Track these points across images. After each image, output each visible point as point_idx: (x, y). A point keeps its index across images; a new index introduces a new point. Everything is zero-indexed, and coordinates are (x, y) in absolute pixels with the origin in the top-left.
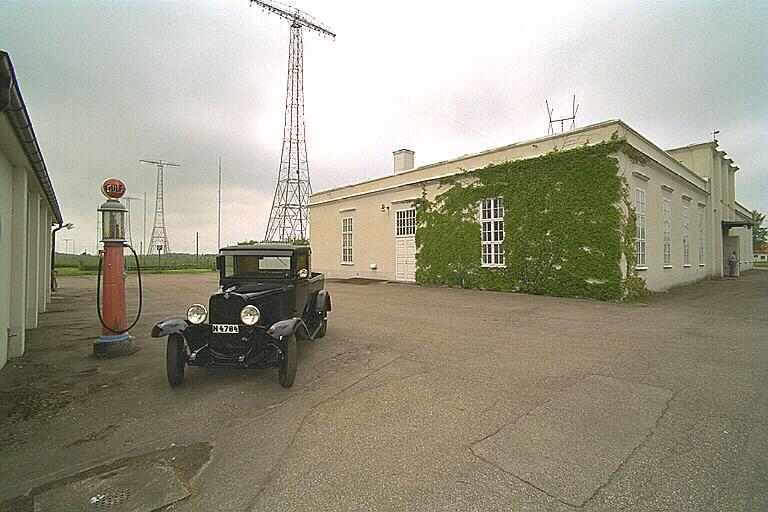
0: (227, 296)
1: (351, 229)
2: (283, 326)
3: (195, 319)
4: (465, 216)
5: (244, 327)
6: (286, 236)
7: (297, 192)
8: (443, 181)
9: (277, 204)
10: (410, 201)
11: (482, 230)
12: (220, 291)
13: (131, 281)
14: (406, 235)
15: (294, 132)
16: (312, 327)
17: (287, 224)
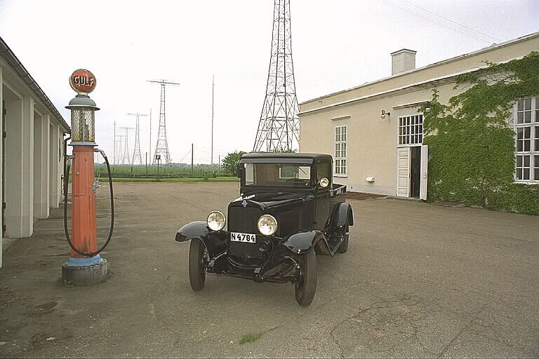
0: (245, 204)
1: (344, 138)
2: (301, 239)
3: (215, 226)
4: (491, 120)
5: (260, 237)
6: (272, 148)
7: (284, 104)
8: (460, 79)
9: (264, 117)
10: (417, 105)
11: (515, 137)
12: (240, 199)
13: (103, 188)
14: (402, 145)
15: (281, 47)
16: (332, 241)
17: (274, 136)
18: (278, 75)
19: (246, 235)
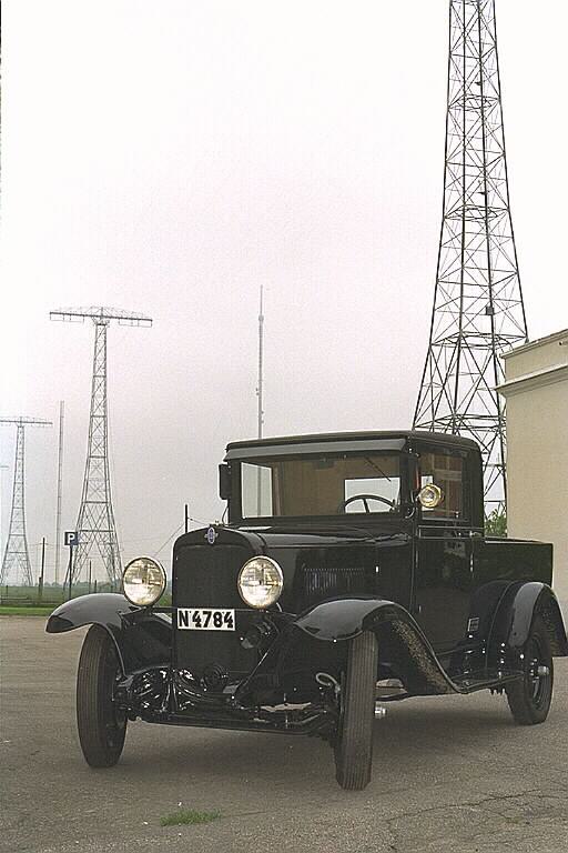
18: (467, 279)
19: (214, 611)
